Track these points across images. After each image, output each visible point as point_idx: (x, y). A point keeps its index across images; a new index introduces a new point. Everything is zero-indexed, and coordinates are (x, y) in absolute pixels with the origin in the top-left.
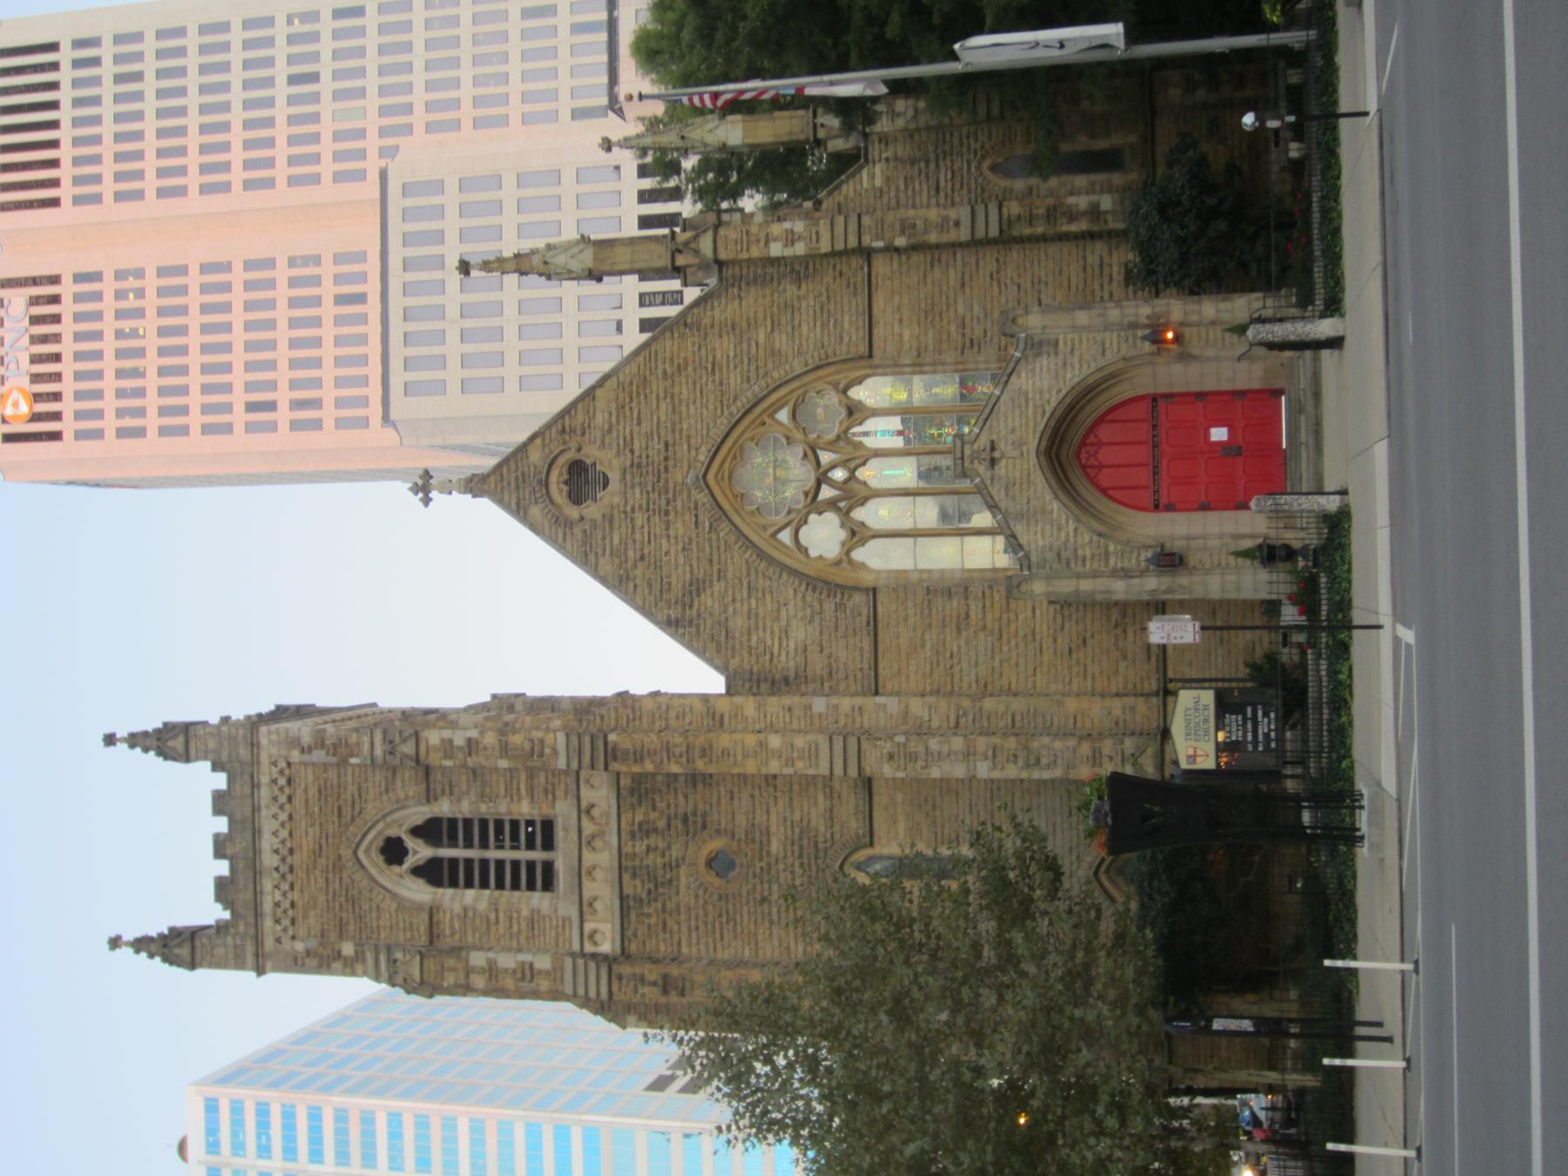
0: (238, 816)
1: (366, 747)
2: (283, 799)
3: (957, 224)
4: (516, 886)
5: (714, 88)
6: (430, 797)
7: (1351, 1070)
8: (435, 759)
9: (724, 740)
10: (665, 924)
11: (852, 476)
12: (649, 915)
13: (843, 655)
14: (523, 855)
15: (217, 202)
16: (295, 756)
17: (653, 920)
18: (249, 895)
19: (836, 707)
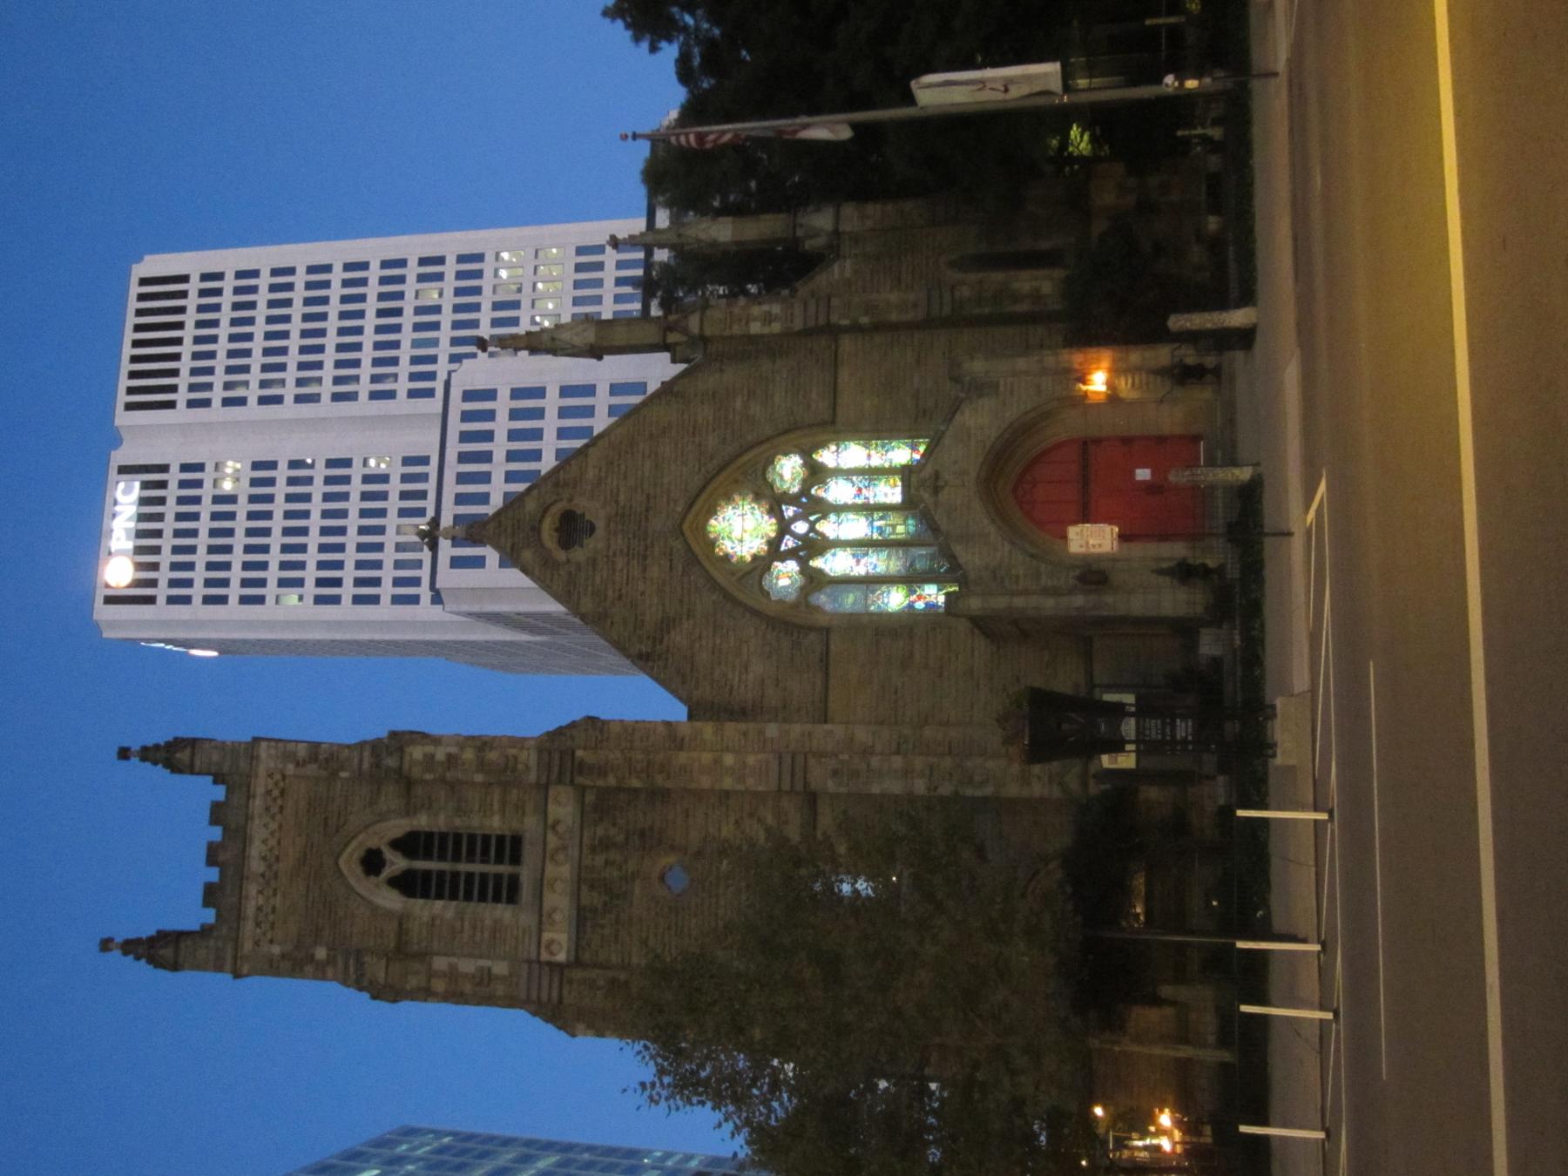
1: (356, 761)
2: (274, 809)
5: (700, 129)
6: (409, 811)
8: (416, 772)
9: (683, 757)
10: (616, 937)
11: (812, 528)
12: (603, 927)
15: (307, 410)
16: (290, 769)
17: (607, 931)
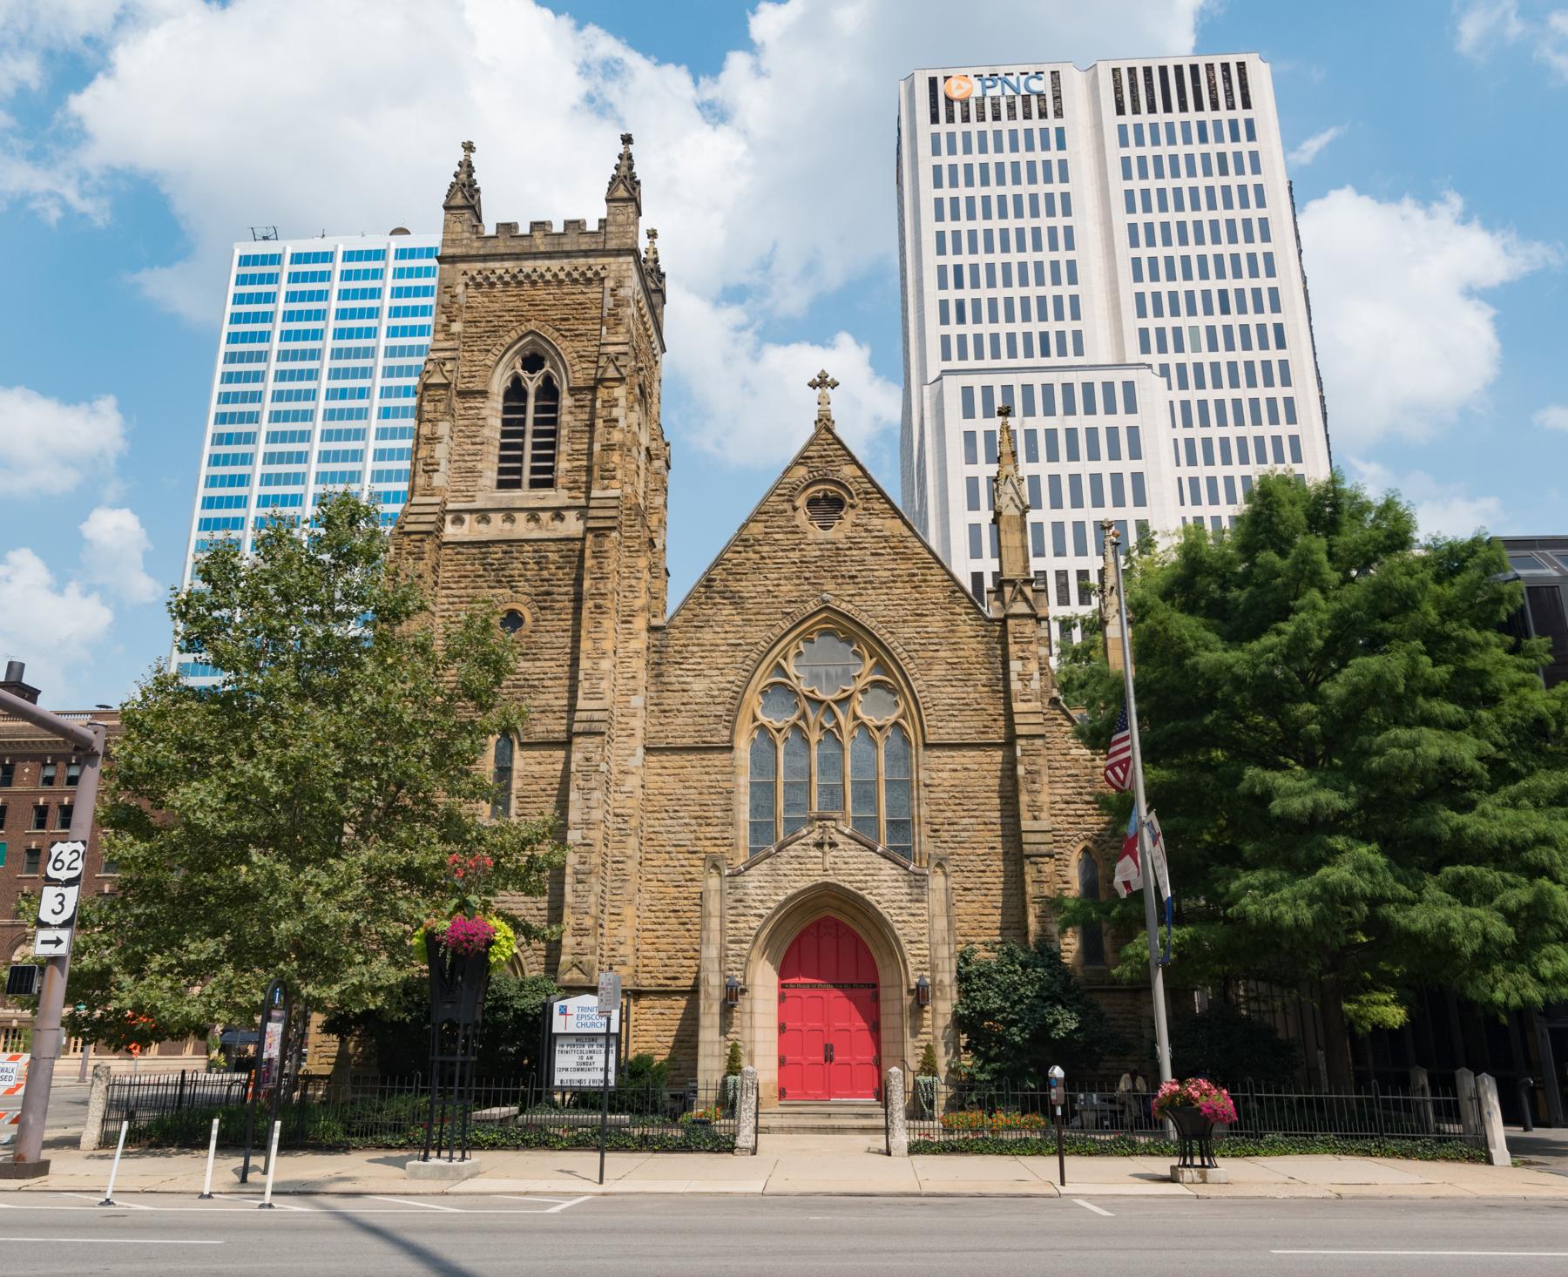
0: (563, 240)
3: (1035, 818)
4: (502, 459)
7: (206, 1146)
8: (602, 393)
13: (679, 721)
14: (527, 464)
17: (469, 567)
18: (502, 250)
19: (634, 715)
